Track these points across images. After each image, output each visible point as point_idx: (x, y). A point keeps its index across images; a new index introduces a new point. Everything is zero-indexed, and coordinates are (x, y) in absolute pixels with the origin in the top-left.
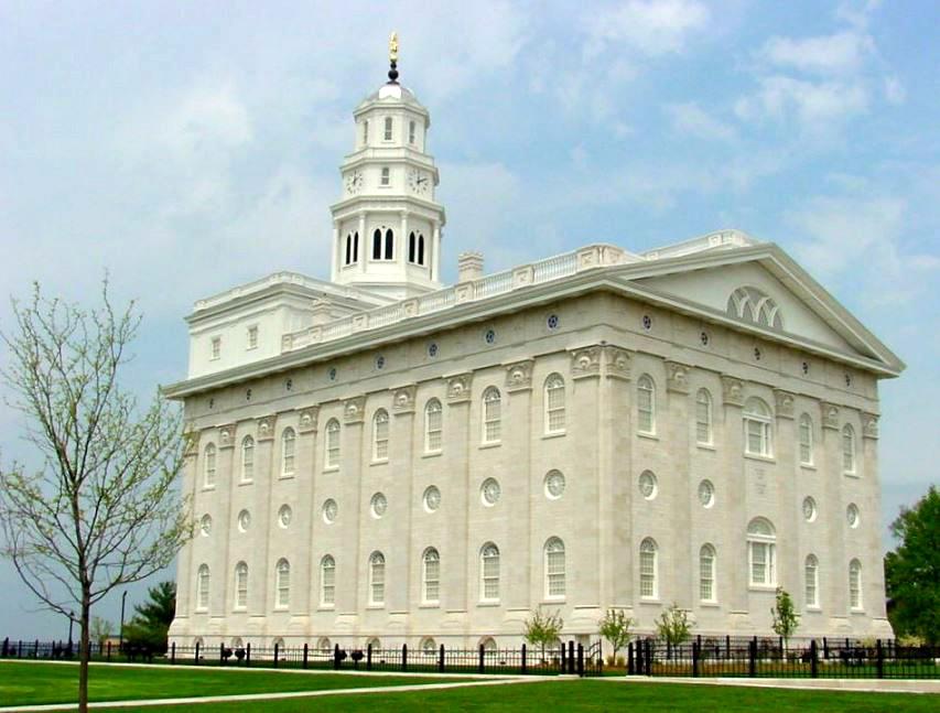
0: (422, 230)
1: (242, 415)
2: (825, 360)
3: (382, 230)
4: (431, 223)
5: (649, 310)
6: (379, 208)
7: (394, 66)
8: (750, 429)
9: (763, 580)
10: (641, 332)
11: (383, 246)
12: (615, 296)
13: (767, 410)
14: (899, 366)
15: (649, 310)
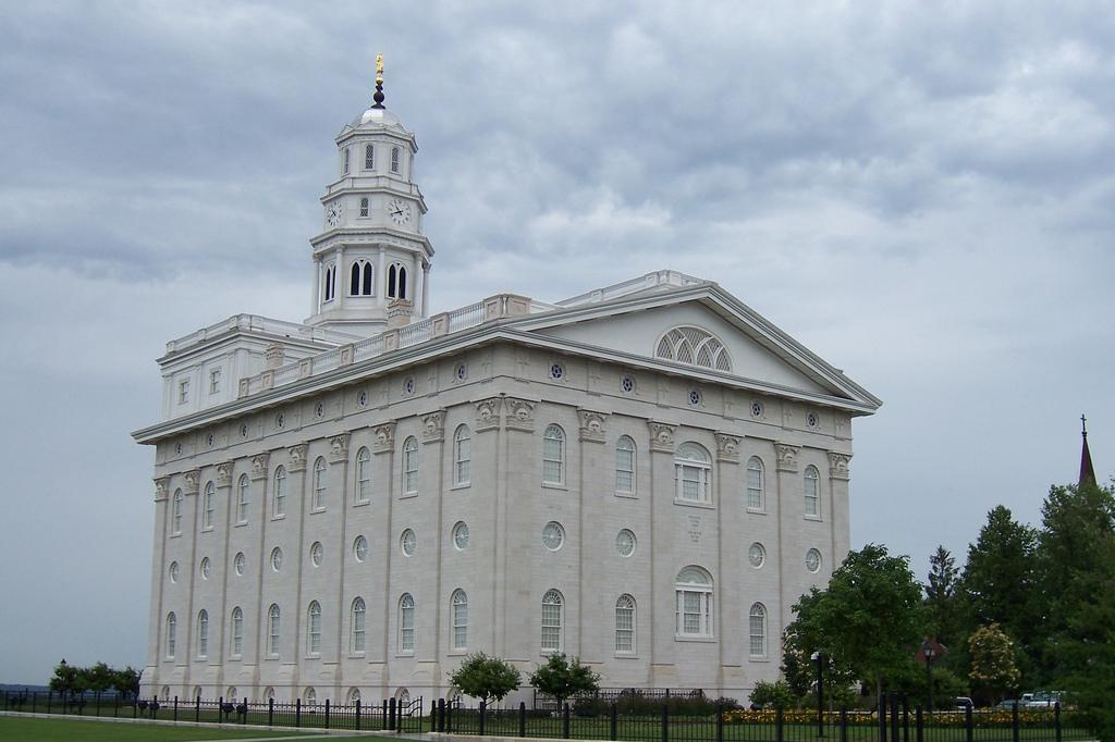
0: (405, 262)
2: (781, 401)
3: (396, 266)
4: (414, 254)
5: (559, 360)
6: (356, 241)
7: (379, 88)
8: (685, 474)
9: (697, 630)
10: (549, 381)
11: (361, 281)
12: (516, 347)
13: (708, 457)
14: (875, 403)
15: (559, 360)
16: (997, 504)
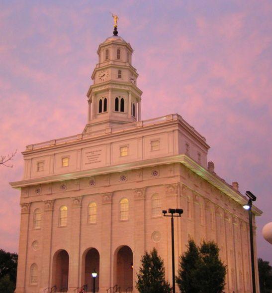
1: (37, 199)
3: (119, 98)
4: (128, 92)
6: (118, 87)
7: (116, 29)
16: (268, 261)
